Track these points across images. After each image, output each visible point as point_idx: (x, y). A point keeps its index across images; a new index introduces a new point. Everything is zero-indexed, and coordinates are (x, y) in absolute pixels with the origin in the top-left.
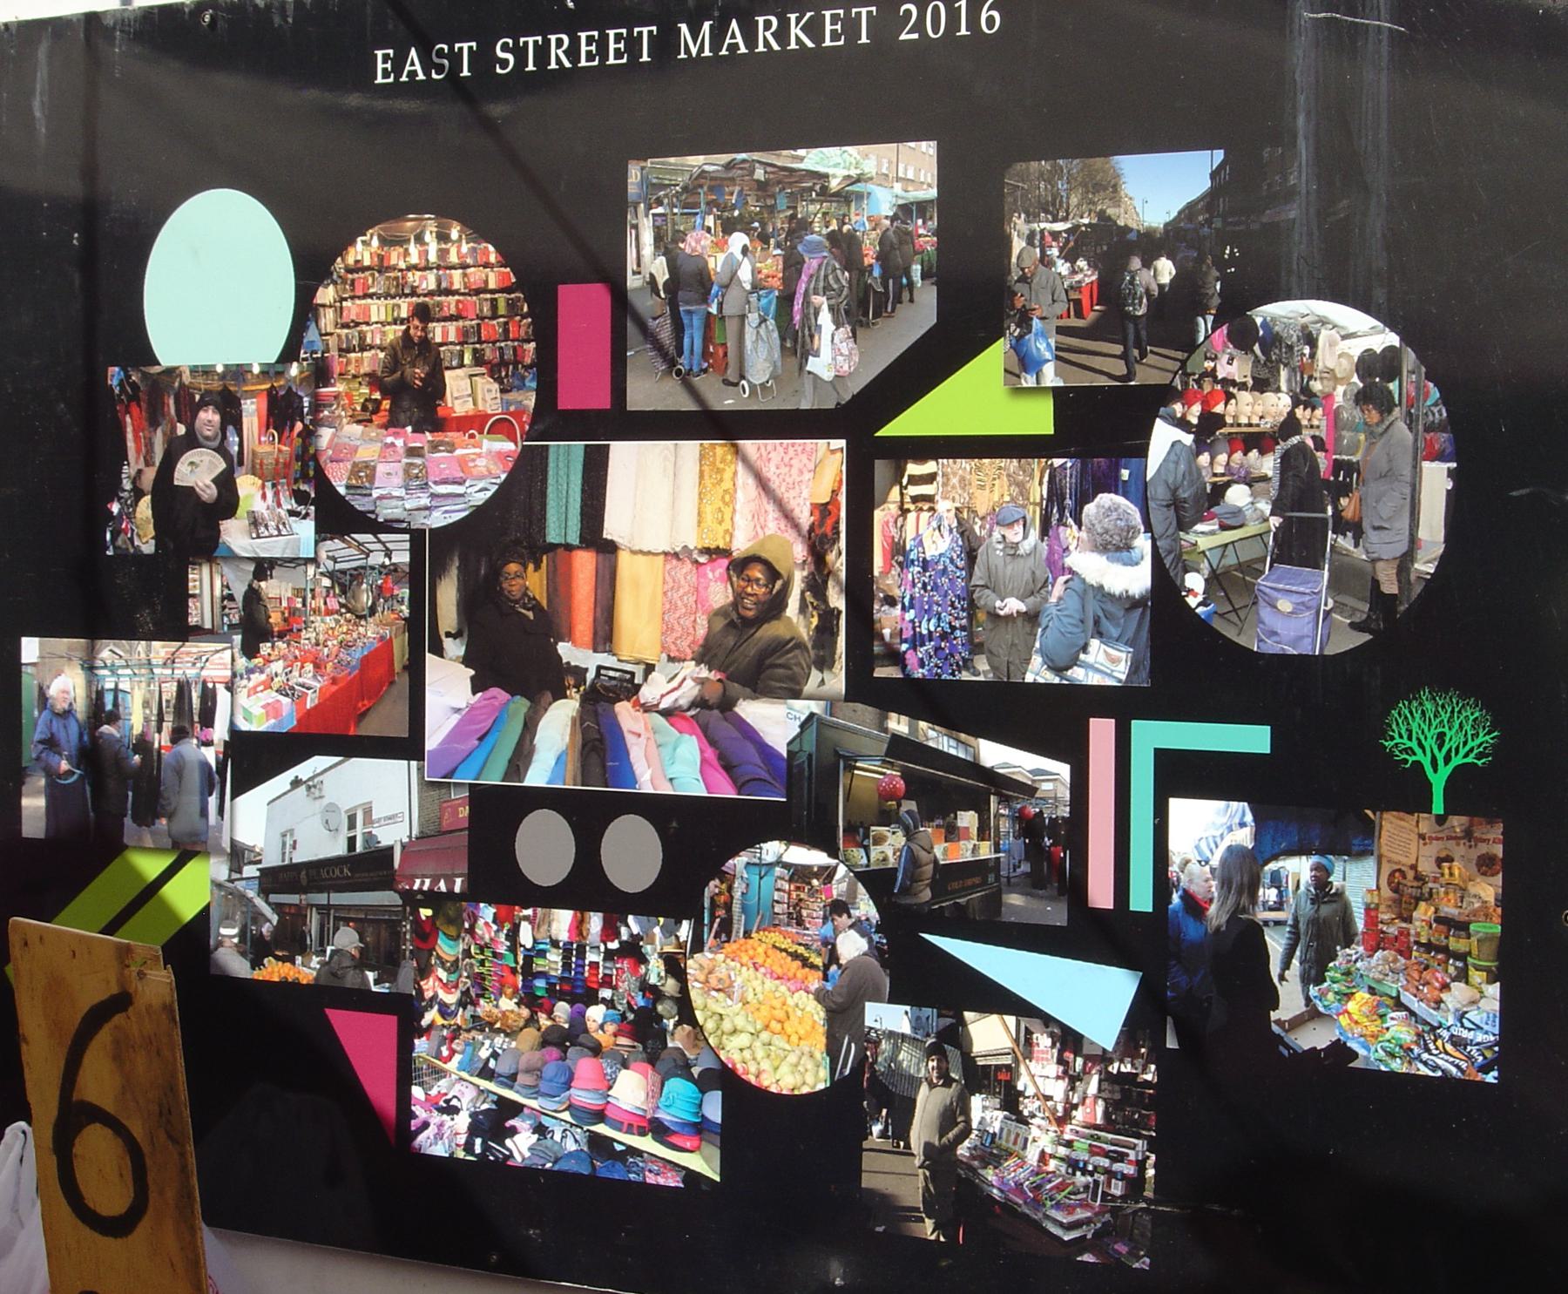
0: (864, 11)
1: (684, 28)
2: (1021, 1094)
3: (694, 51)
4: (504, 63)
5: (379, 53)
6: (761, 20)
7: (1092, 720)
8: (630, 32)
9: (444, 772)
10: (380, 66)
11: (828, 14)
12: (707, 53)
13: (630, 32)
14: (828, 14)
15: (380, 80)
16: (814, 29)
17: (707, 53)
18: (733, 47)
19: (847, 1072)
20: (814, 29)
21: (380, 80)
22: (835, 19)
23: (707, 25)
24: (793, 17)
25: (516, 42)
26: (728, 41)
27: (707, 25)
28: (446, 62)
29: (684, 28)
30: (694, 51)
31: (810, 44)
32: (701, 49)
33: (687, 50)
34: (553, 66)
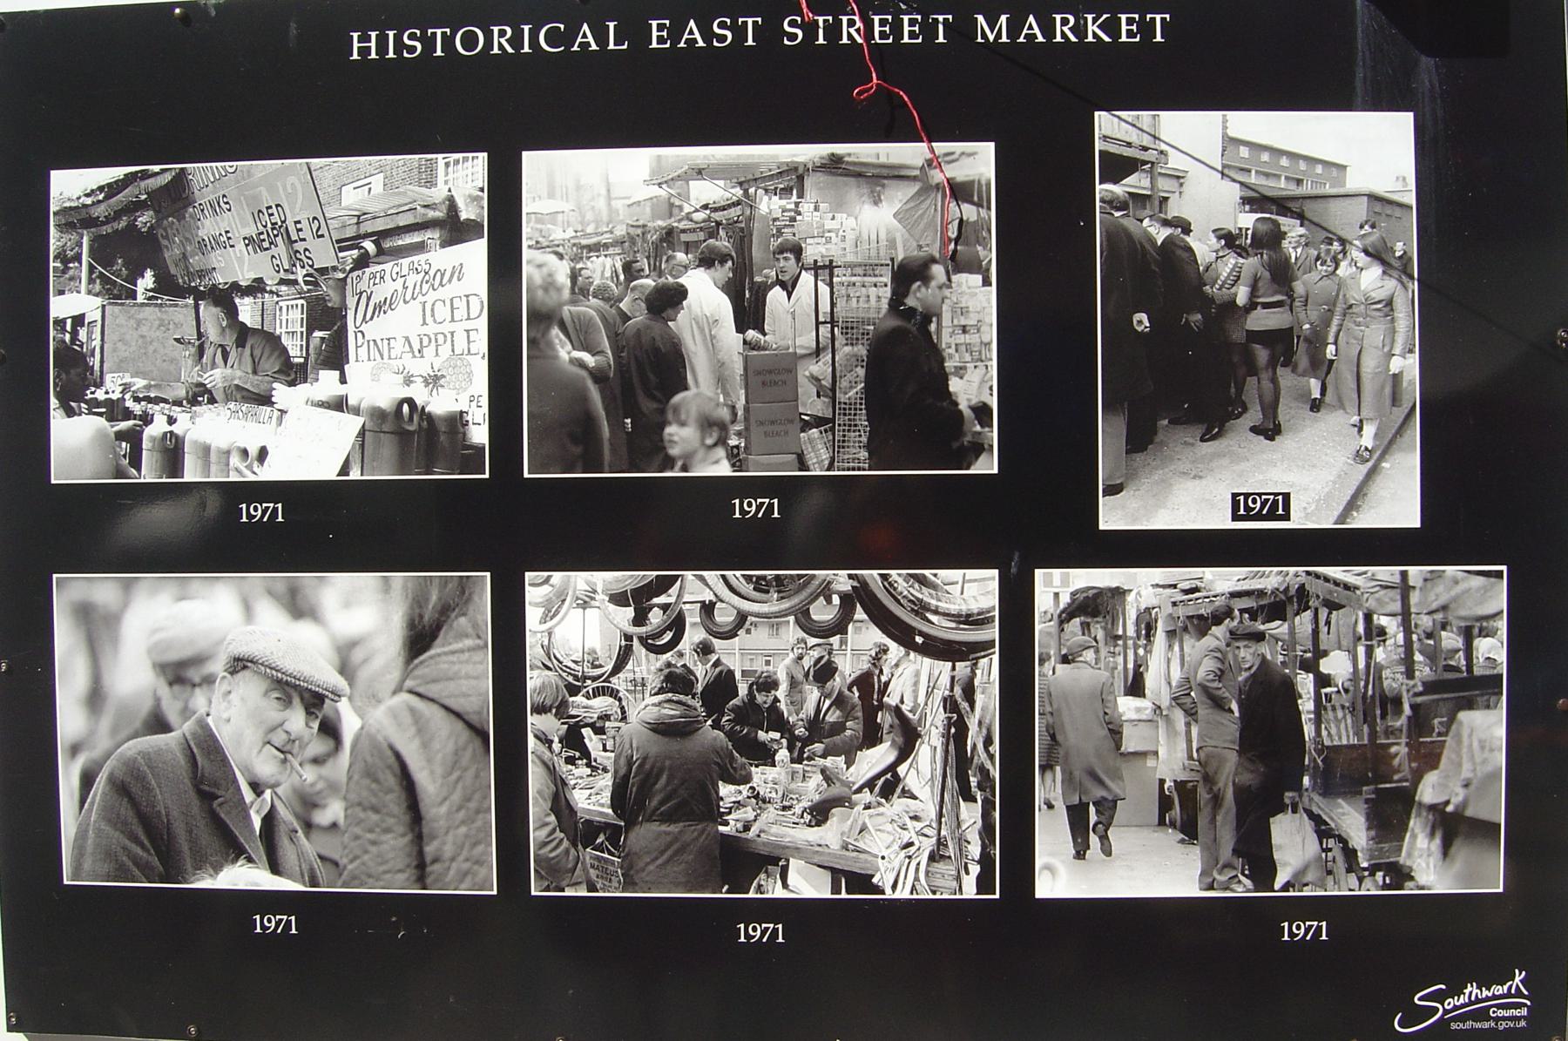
0: (439, 32)
1: (980, 18)
2: (979, 862)
3: (991, 38)
4: (793, 37)
5: (654, 23)
6: (1058, 17)
7: (1418, 525)
8: (1143, 17)
9: (478, 742)
10: (655, 34)
11: (1123, 17)
12: (1004, 39)
13: (1143, 17)
14: (1123, 17)
15: (654, 45)
16: (1111, 27)
17: (1004, 39)
18: (1032, 37)
19: (1454, 1026)
20: (1111, 27)
21: (654, 45)
22: (1130, 22)
23: (1003, 18)
24: (1090, 17)
25: (424, 33)
26: (686, 36)
27: (1003, 18)
28: (407, 41)
29: (980, 18)
30: (991, 38)
31: (1107, 39)
32: (999, 35)
33: (984, 35)
34: (1090, 39)
